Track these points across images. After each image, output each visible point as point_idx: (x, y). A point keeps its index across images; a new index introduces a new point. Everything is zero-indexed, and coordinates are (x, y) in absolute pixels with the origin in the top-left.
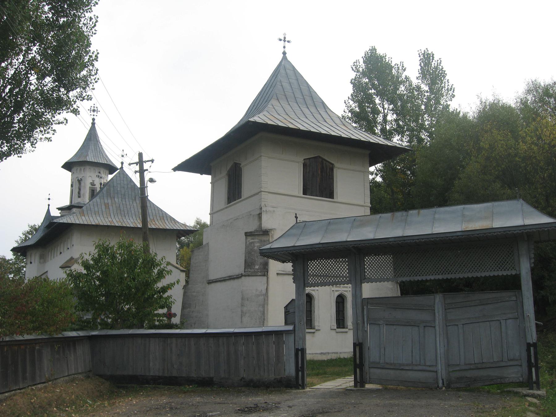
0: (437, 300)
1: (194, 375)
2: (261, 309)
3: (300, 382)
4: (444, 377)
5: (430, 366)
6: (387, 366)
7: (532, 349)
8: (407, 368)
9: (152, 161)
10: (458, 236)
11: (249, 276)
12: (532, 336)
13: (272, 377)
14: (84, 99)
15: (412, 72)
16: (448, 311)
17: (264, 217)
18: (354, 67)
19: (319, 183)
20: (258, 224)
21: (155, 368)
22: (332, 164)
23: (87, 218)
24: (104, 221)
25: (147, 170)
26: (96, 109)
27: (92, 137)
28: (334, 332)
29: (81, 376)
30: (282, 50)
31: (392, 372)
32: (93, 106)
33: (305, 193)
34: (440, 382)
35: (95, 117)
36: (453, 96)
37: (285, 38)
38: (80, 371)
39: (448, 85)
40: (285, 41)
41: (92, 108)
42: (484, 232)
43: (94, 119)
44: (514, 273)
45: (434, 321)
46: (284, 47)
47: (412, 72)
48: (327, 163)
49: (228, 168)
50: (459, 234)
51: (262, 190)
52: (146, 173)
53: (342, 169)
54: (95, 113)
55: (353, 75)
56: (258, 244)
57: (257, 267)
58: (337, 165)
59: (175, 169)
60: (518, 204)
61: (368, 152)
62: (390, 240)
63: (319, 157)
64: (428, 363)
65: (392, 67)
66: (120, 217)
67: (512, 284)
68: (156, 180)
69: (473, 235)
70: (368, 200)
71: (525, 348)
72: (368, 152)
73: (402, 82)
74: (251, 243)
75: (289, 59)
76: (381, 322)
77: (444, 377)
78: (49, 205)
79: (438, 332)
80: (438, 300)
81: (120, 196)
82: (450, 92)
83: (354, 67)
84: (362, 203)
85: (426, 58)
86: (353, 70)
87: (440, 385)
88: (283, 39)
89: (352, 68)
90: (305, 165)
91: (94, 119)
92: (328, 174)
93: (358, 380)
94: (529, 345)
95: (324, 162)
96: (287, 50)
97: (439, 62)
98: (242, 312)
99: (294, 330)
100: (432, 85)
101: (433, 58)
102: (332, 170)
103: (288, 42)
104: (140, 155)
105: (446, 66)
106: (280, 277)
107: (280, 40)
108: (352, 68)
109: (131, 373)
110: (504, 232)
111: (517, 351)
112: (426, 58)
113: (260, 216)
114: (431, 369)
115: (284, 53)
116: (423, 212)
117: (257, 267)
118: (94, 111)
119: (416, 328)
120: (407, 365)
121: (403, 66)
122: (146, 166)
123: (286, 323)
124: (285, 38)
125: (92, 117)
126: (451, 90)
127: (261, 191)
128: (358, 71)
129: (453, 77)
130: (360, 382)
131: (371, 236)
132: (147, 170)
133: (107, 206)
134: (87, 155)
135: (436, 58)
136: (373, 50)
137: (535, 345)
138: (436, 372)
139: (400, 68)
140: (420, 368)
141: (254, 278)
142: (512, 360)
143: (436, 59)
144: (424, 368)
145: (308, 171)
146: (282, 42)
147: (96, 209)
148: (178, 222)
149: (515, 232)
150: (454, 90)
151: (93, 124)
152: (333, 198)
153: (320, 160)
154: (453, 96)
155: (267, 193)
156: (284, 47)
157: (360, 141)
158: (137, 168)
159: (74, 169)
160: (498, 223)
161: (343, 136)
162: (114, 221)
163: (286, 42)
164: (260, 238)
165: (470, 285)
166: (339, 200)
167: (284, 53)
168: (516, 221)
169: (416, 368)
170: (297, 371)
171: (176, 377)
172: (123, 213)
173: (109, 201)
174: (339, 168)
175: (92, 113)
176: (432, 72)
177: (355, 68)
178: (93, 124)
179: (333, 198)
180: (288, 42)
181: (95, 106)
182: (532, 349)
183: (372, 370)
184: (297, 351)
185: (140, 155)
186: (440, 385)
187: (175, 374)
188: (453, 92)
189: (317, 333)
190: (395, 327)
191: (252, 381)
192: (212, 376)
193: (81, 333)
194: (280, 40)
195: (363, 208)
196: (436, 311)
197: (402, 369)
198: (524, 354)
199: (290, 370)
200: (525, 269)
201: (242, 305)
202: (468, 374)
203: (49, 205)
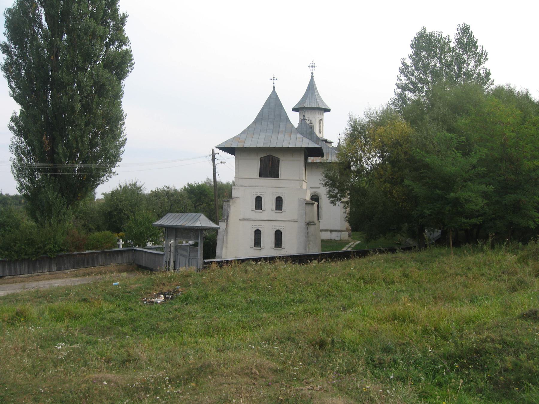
27: (311, 88)
28: (273, 250)
30: (273, 85)
33: (260, 176)
35: (313, 71)
43: (312, 73)
54: (313, 68)
58: (281, 158)
91: (312, 73)
102: (279, 161)
106: (241, 221)
115: (274, 87)
118: (312, 67)
121: (449, 39)
122: (216, 156)
125: (311, 71)
134: (305, 102)
136: (424, 29)
150: (487, 54)
151: (312, 77)
167: (274, 87)
175: (311, 69)
178: (312, 77)
179: (278, 177)
188: (486, 56)
189: (262, 250)
193: (94, 251)
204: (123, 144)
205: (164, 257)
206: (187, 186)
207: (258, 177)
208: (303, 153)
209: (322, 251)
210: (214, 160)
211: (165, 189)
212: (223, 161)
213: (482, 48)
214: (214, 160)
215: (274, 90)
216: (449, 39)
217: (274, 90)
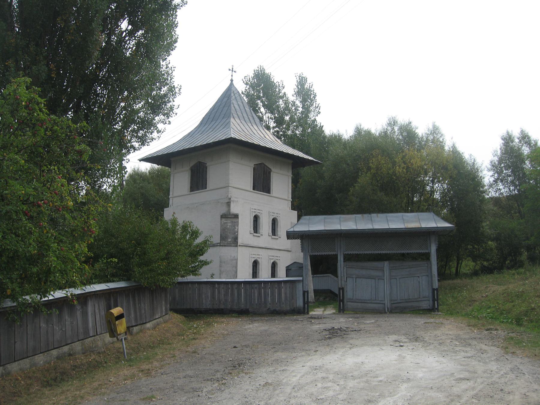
0: (385, 265)
1: (235, 307)
2: (234, 269)
4: (389, 306)
11: (225, 246)
12: (436, 285)
13: (288, 308)
14: (166, 123)
17: (232, 205)
20: (227, 209)
21: (207, 304)
22: (270, 169)
31: (360, 304)
34: (387, 309)
40: (232, 71)
44: (334, 253)
45: (384, 276)
46: (232, 76)
47: (289, 90)
49: (192, 165)
53: (276, 173)
56: (230, 224)
57: (229, 240)
58: (273, 170)
59: (140, 160)
60: (431, 215)
61: (291, 162)
64: (380, 299)
67: (426, 257)
71: (431, 291)
72: (291, 162)
73: (282, 97)
74: (225, 223)
77: (389, 306)
80: (386, 263)
82: (317, 109)
84: (286, 198)
85: (302, 82)
87: (386, 311)
94: (434, 290)
97: (311, 85)
98: (220, 271)
99: (303, 280)
100: (303, 101)
102: (270, 173)
103: (235, 72)
105: (316, 89)
107: (230, 70)
109: (188, 307)
111: (427, 293)
112: (302, 82)
113: (228, 204)
114: (382, 302)
115: (232, 80)
116: (380, 215)
117: (229, 240)
119: (374, 280)
120: (369, 300)
123: (287, 276)
129: (321, 99)
131: (354, 227)
135: (308, 81)
137: (437, 289)
138: (384, 304)
140: (375, 302)
141: (229, 248)
144: (378, 302)
152: (206, 188)
156: (232, 76)
157: (288, 154)
160: (424, 225)
161: (243, 140)
164: (232, 220)
165: (403, 257)
166: (274, 195)
167: (232, 80)
168: (432, 224)
169: (373, 302)
170: (304, 303)
171: (222, 309)
174: (274, 172)
176: (305, 94)
179: (206, 188)
180: (235, 72)
183: (348, 303)
184: (304, 292)
186: (386, 311)
187: (222, 307)
191: (275, 310)
194: (230, 70)
198: (431, 294)
199: (300, 303)
200: (433, 249)
201: (220, 266)
202: (401, 305)
208: (291, 167)
217: (232, 84)
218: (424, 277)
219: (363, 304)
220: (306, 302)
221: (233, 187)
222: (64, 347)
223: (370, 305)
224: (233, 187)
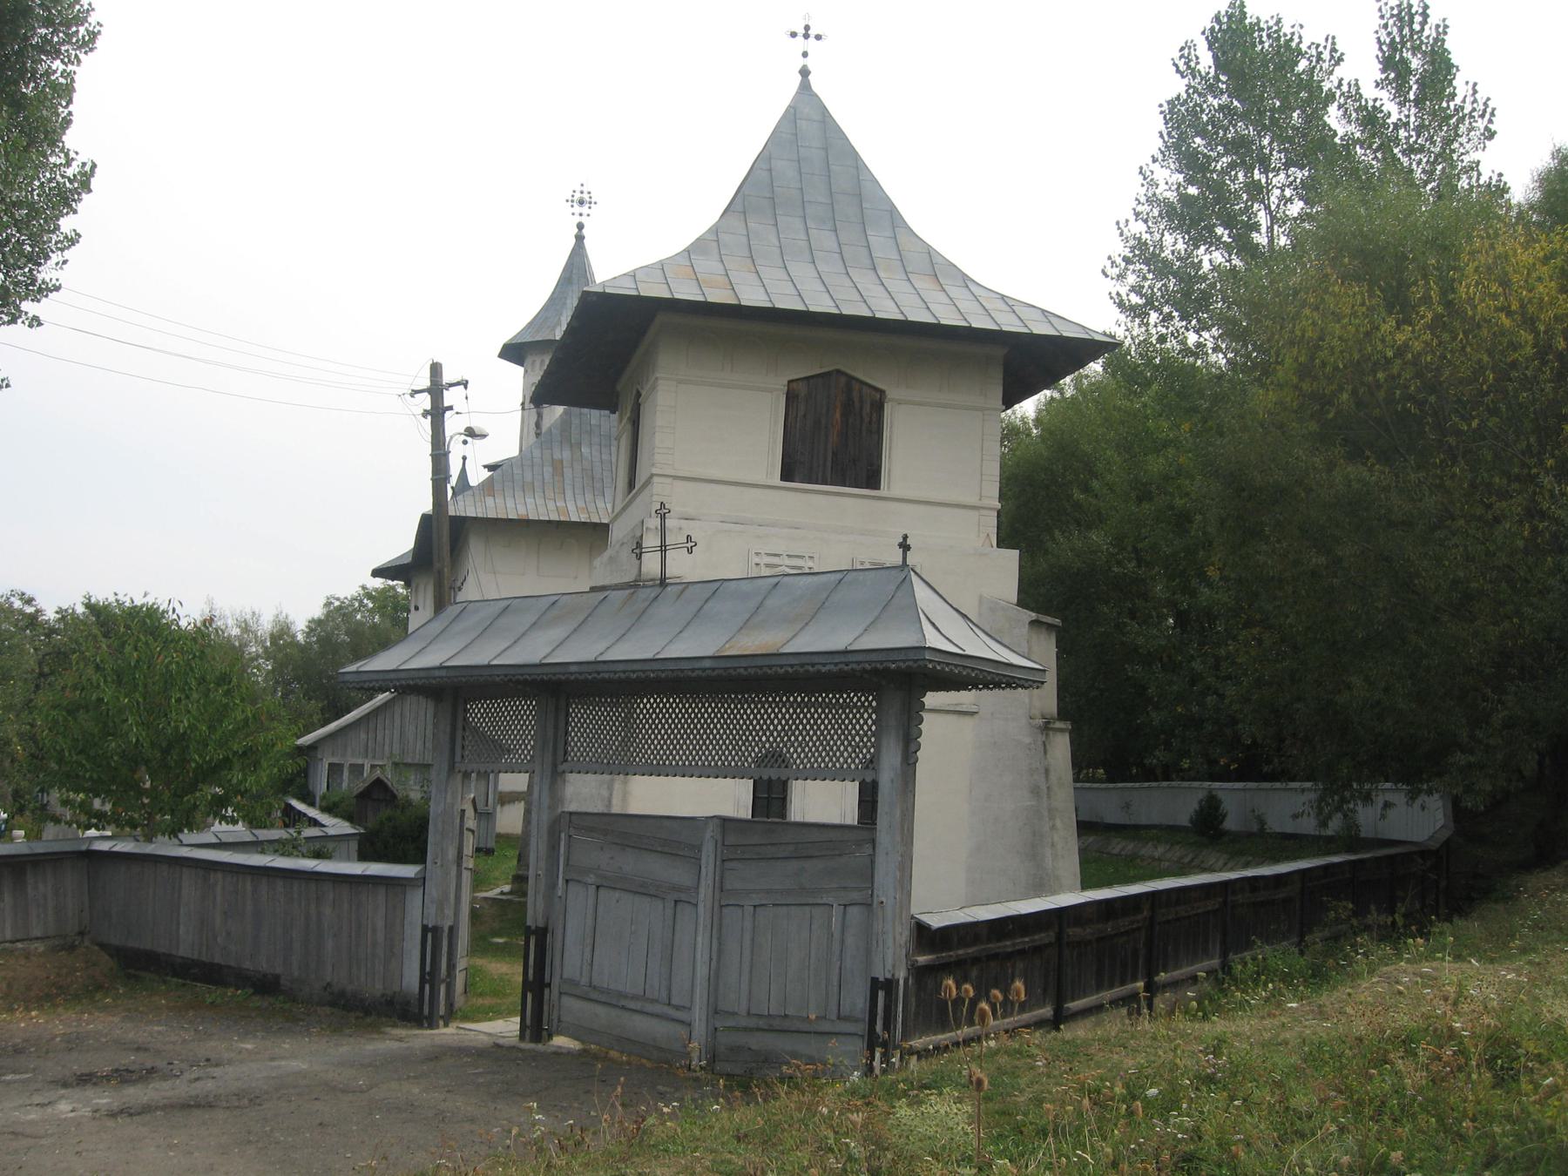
2: (605, 793)
3: (426, 1011)
5: (677, 1008)
6: (594, 995)
7: (881, 994)
8: (632, 1005)
9: (465, 384)
10: (704, 670)
13: (378, 988)
15: (1361, 69)
16: (728, 865)
18: (1181, 64)
19: (834, 442)
21: (186, 944)
22: (882, 392)
23: (540, 501)
24: (542, 510)
25: (451, 408)
26: (586, 196)
29: (40, 947)
30: (801, 62)
31: (601, 1011)
32: (578, 189)
33: (787, 475)
35: (584, 219)
36: (1490, 135)
37: (807, 28)
38: (37, 932)
39: (1475, 101)
41: (578, 195)
42: (759, 662)
43: (580, 226)
46: (805, 55)
48: (865, 390)
50: (707, 664)
51: (654, 471)
52: (448, 414)
54: (585, 210)
55: (1178, 86)
58: (892, 393)
62: (573, 669)
63: (838, 371)
65: (1300, 53)
66: (589, 497)
68: (487, 430)
69: (693, 670)
70: (993, 490)
75: (815, 88)
76: (591, 879)
78: (464, 458)
79: (701, 920)
81: (596, 440)
83: (1181, 64)
86: (1178, 71)
88: (801, 31)
89: (1175, 65)
90: (791, 398)
91: (580, 226)
92: (867, 420)
93: (528, 1022)
94: (875, 984)
95: (856, 386)
96: (810, 63)
101: (1425, 16)
102: (879, 407)
103: (818, 37)
104: (436, 369)
107: (794, 35)
108: (1175, 65)
109: (148, 947)
110: (802, 665)
115: (805, 72)
118: (581, 202)
120: (634, 998)
121: (1334, 50)
122: (449, 397)
124: (807, 28)
125: (577, 219)
126: (1482, 116)
127: (652, 475)
128: (1194, 73)
130: (536, 1028)
132: (451, 408)
133: (558, 467)
139: (1326, 55)
140: (658, 1009)
142: (846, 1019)
143: (1433, 20)
145: (801, 413)
146: (800, 38)
147: (528, 477)
148: (965, 280)
149: (824, 669)
150: (1492, 114)
151: (580, 238)
152: (876, 486)
153: (843, 380)
154: (1490, 135)
155: (669, 480)
156: (805, 55)
158: (425, 401)
159: (528, 361)
162: (571, 507)
163: (812, 39)
166: (896, 491)
167: (805, 72)
169: (649, 1008)
171: (220, 966)
172: (598, 485)
173: (567, 454)
175: (577, 209)
176: (1418, 63)
177: (1187, 68)
178: (580, 238)
179: (876, 486)
180: (818, 37)
181: (585, 189)
182: (881, 994)
183: (566, 1000)
184: (425, 929)
185: (436, 369)
190: (617, 894)
191: (342, 993)
192: (279, 970)
194: (794, 35)
195: (975, 514)
196: (703, 861)
197: (623, 1007)
202: (756, 1042)
203: (464, 458)
204: (65, 199)
205: (414, 899)
206: (80, 609)
207: (777, 481)
208: (998, 375)
209: (1086, 885)
210: (437, 413)
211: (17, 604)
212: (477, 424)
213: (1475, 92)
214: (437, 413)
215: (805, 86)
216: (1334, 50)
217: (805, 86)
218: (853, 910)
219: (614, 1013)
220: (428, 977)
221: (676, 478)
222: (1156, 819)
223: (637, 1018)
224: (676, 478)
